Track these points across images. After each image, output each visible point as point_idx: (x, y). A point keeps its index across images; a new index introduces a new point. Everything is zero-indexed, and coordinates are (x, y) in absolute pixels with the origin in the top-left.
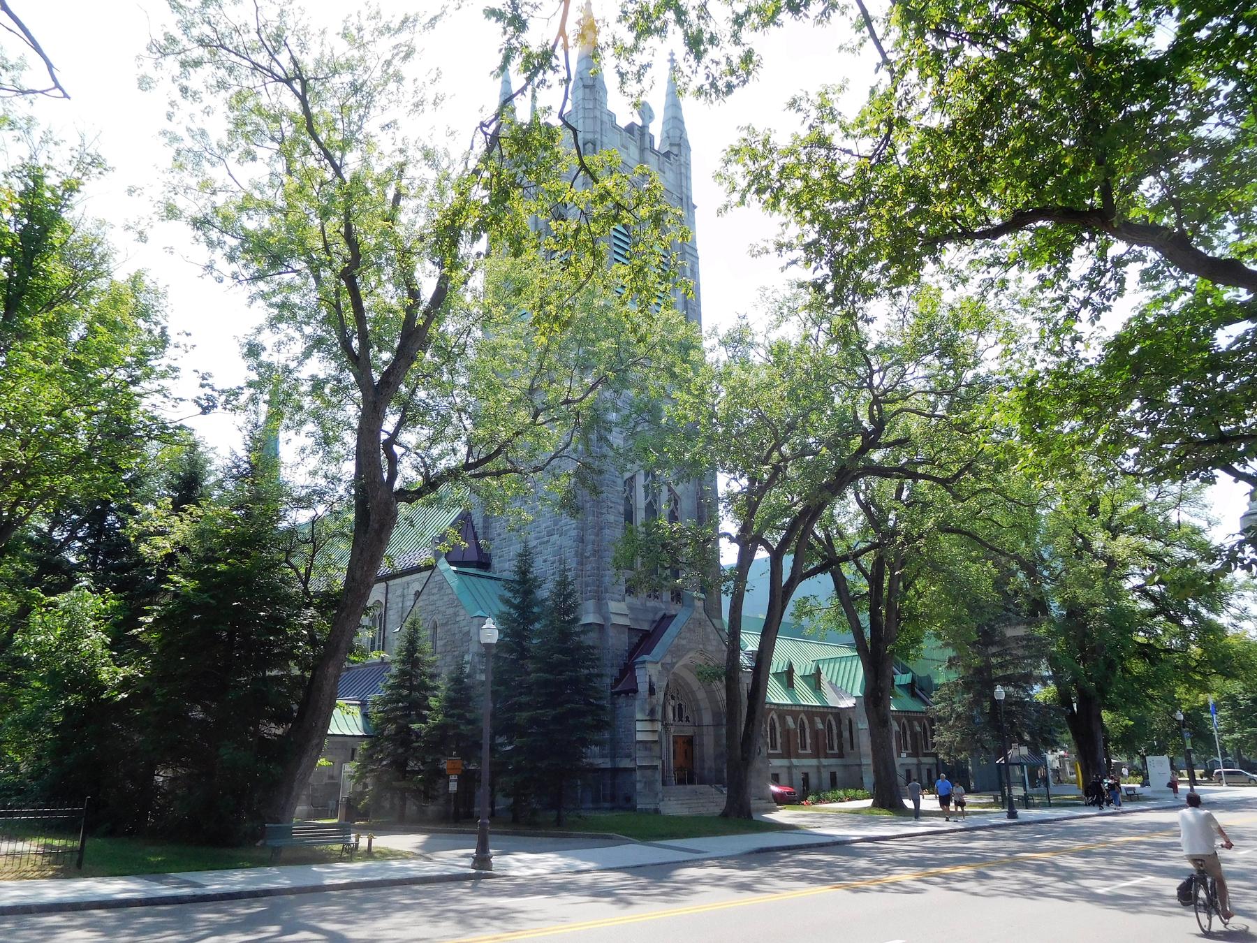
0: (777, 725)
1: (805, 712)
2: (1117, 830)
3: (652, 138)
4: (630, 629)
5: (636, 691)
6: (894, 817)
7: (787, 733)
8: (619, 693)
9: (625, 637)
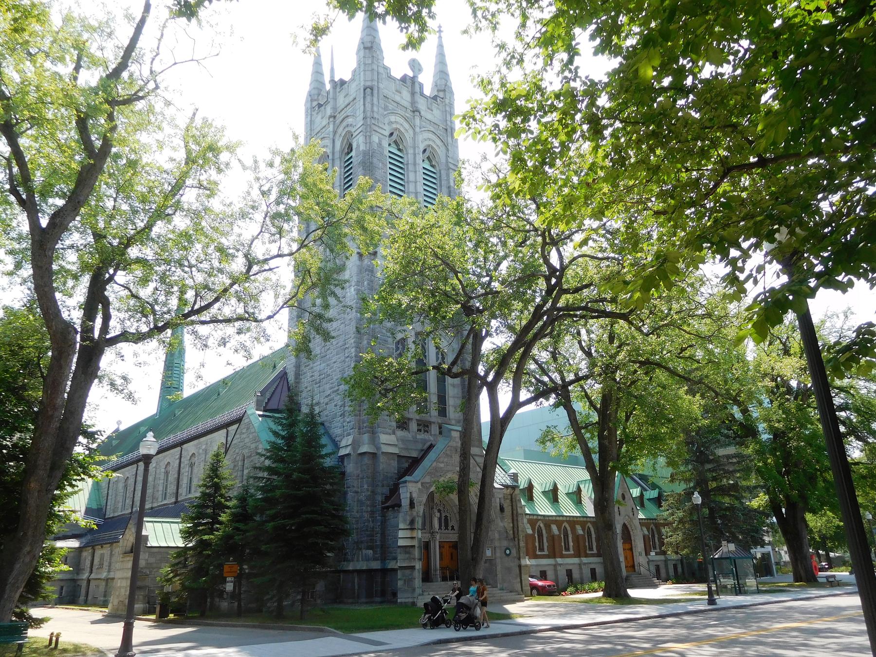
0: (544, 532)
1: (567, 521)
2: (784, 615)
3: (421, 86)
4: (399, 456)
5: (399, 506)
6: (617, 603)
7: (552, 538)
8: (387, 508)
9: (394, 464)
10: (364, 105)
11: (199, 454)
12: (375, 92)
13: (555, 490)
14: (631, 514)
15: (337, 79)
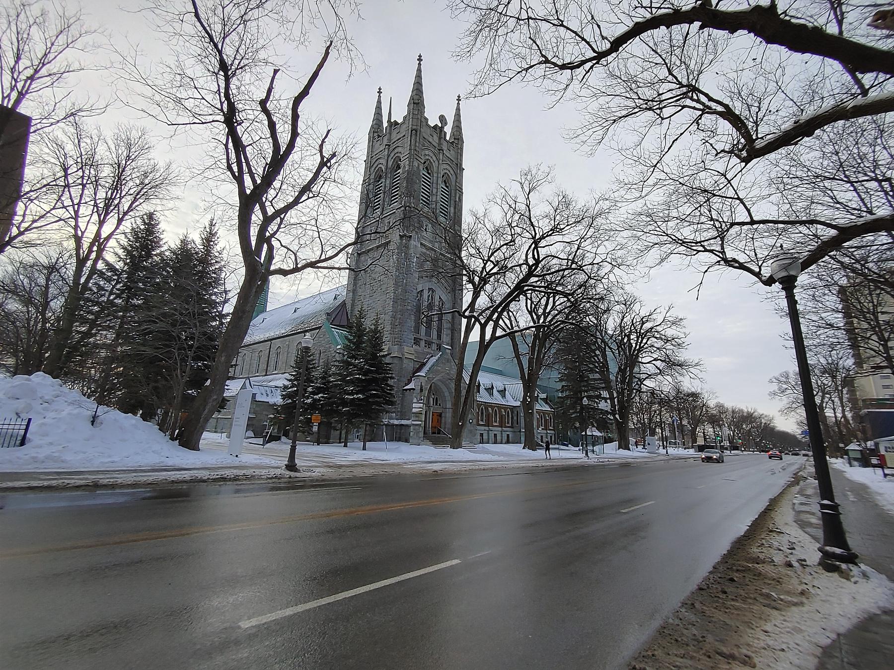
3: (445, 133)
10: (411, 141)
11: (284, 347)
12: (418, 133)
15: (392, 121)
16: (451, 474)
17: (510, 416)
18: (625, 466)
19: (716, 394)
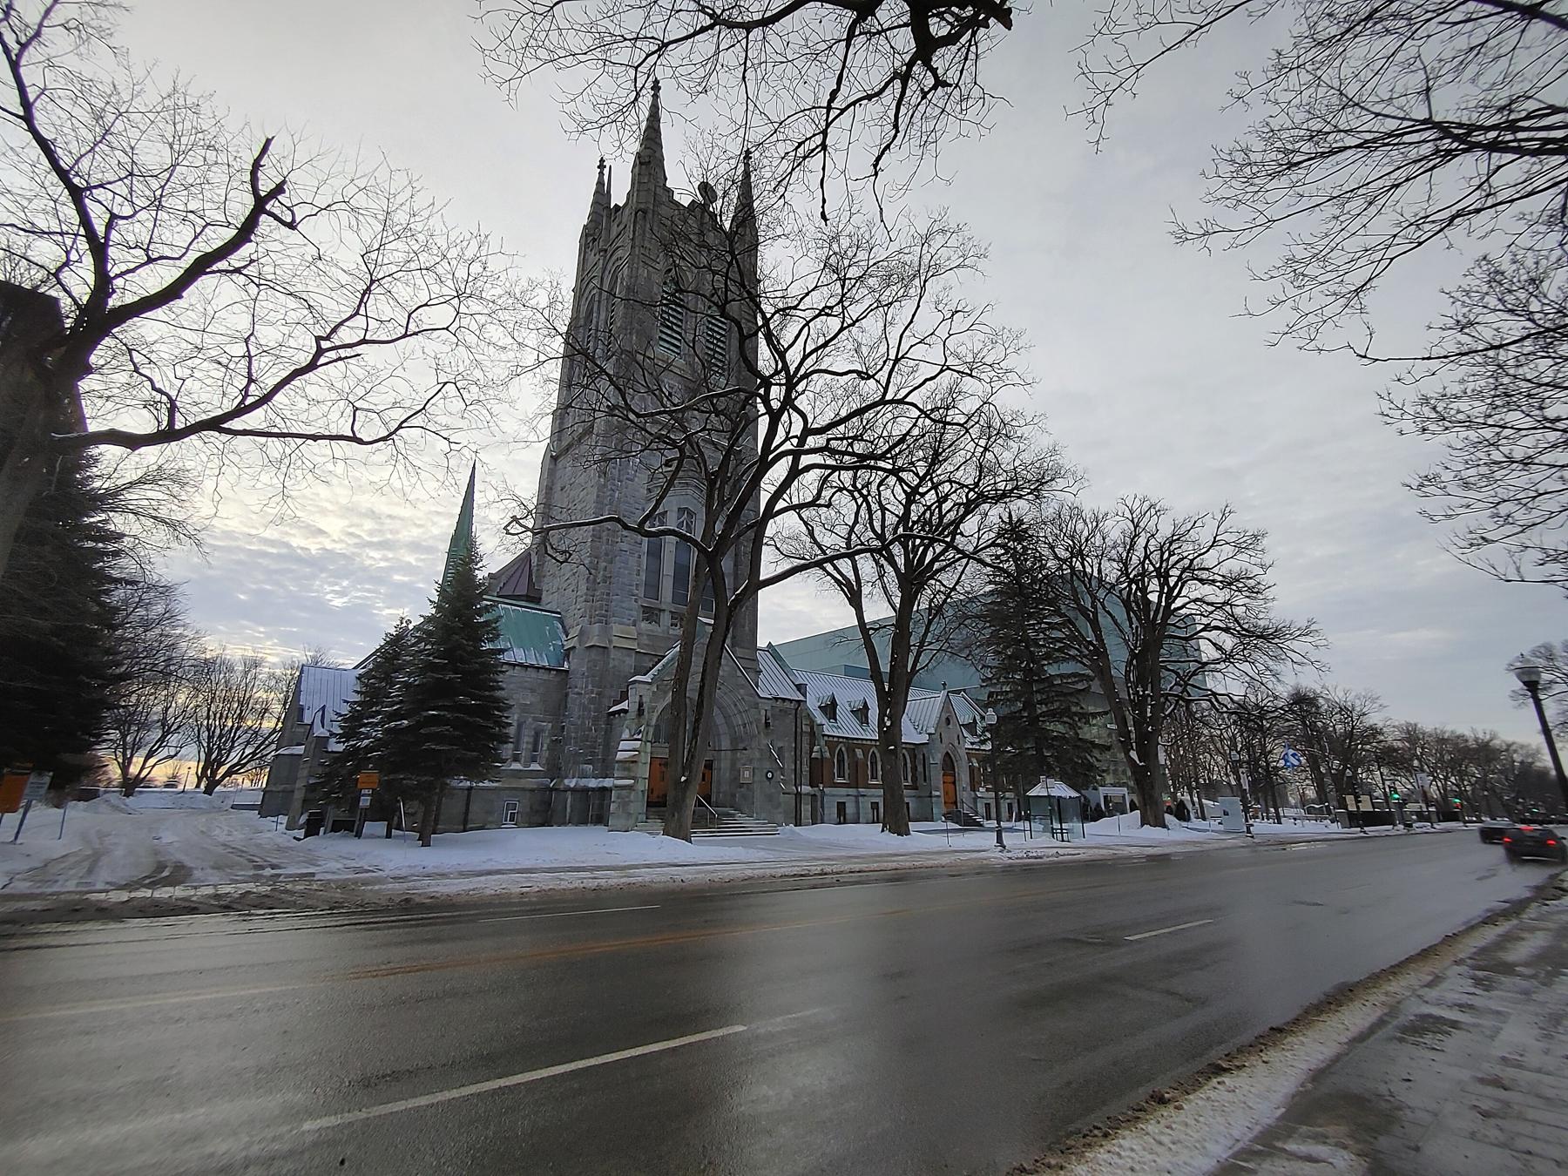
7: (855, 764)
13: (834, 704)
14: (956, 744)
16: (475, 905)
17: (909, 765)
18: (1160, 861)
19: (1380, 702)
